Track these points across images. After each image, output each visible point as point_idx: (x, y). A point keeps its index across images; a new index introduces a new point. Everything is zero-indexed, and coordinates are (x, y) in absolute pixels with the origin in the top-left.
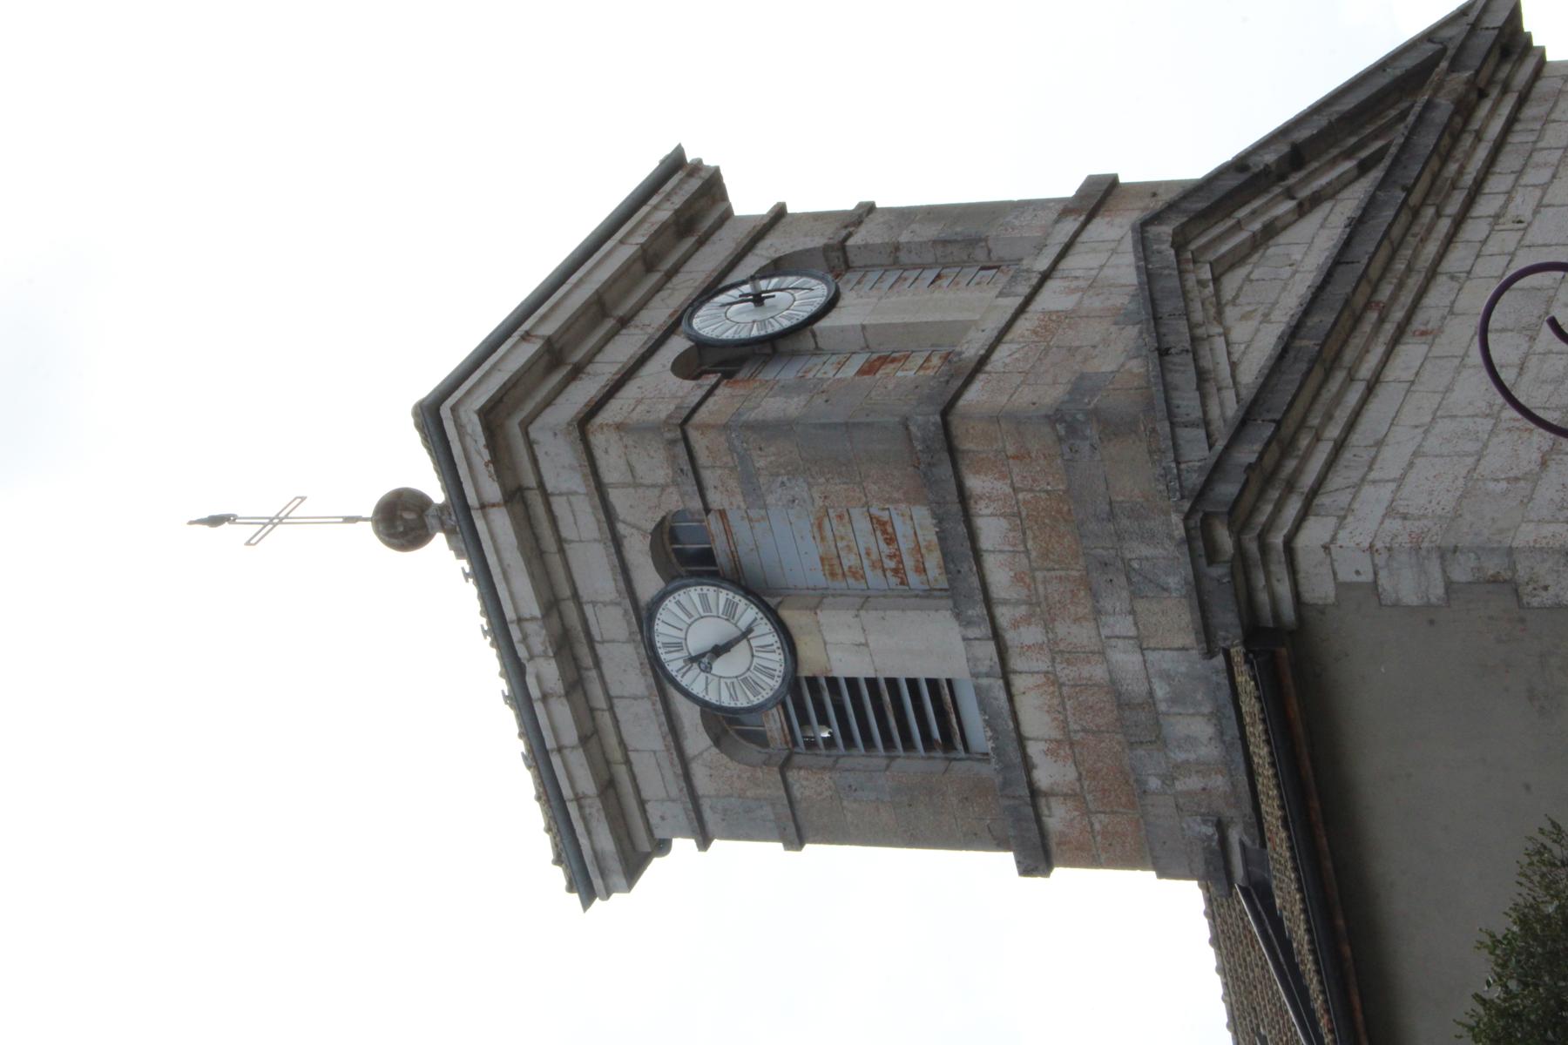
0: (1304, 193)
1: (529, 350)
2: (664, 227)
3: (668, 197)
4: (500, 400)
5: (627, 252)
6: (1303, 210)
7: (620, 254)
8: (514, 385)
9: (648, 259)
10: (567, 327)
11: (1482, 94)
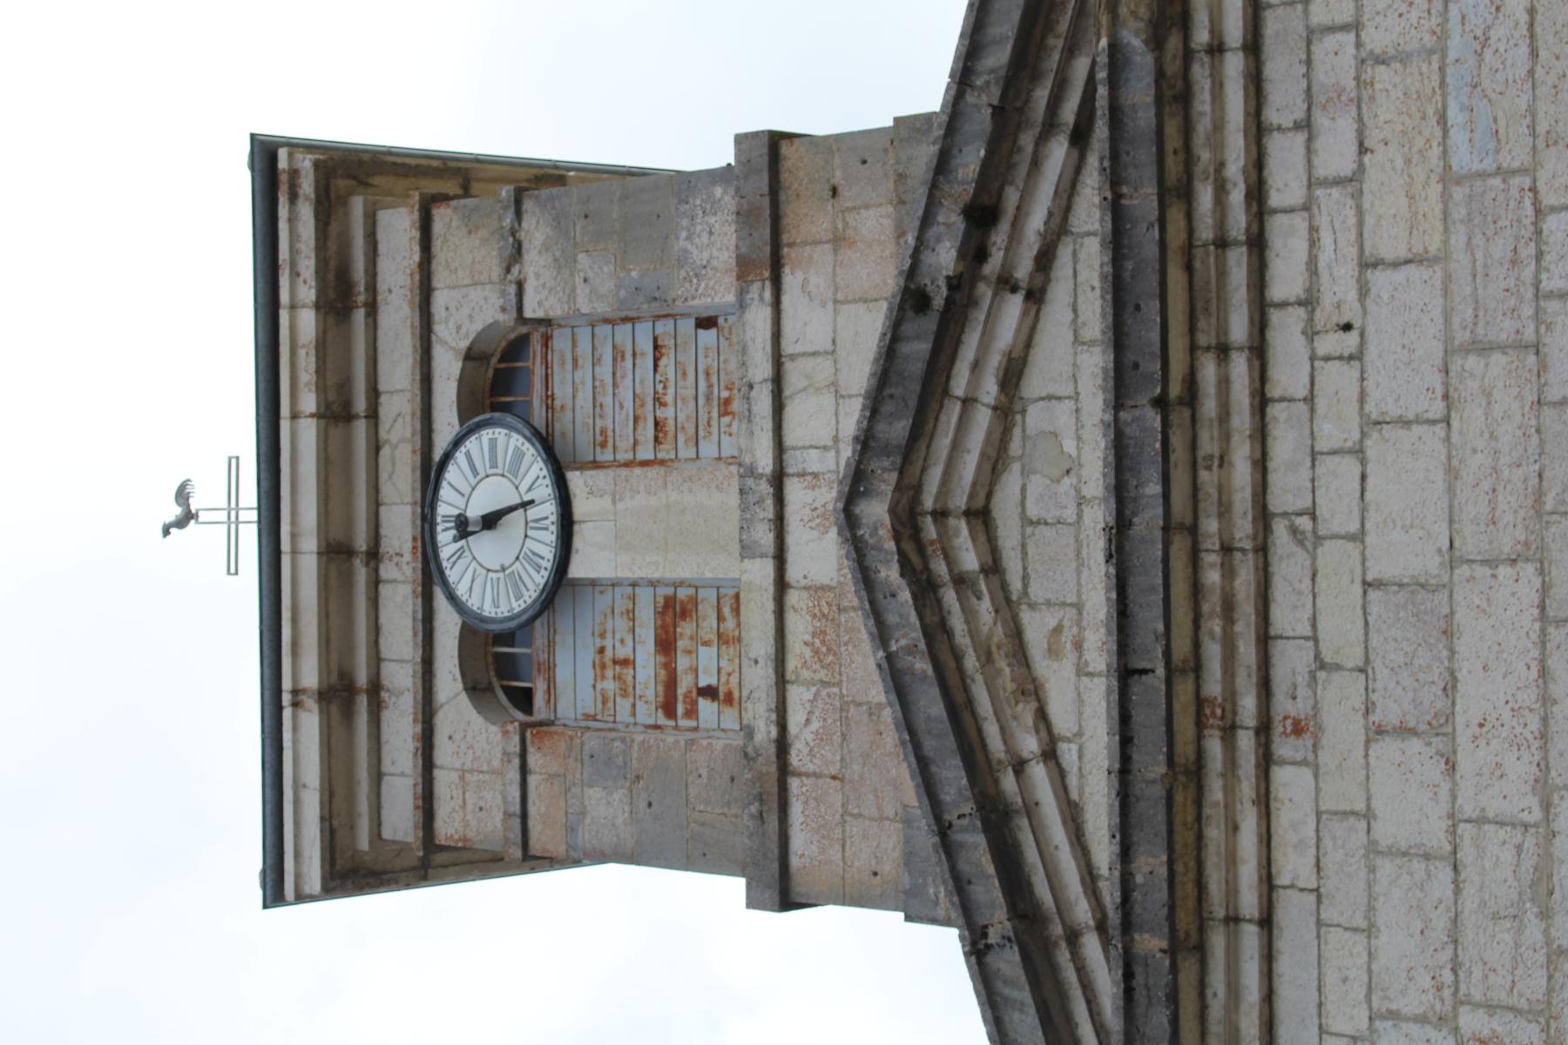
2: (321, 345)
8: (331, 794)
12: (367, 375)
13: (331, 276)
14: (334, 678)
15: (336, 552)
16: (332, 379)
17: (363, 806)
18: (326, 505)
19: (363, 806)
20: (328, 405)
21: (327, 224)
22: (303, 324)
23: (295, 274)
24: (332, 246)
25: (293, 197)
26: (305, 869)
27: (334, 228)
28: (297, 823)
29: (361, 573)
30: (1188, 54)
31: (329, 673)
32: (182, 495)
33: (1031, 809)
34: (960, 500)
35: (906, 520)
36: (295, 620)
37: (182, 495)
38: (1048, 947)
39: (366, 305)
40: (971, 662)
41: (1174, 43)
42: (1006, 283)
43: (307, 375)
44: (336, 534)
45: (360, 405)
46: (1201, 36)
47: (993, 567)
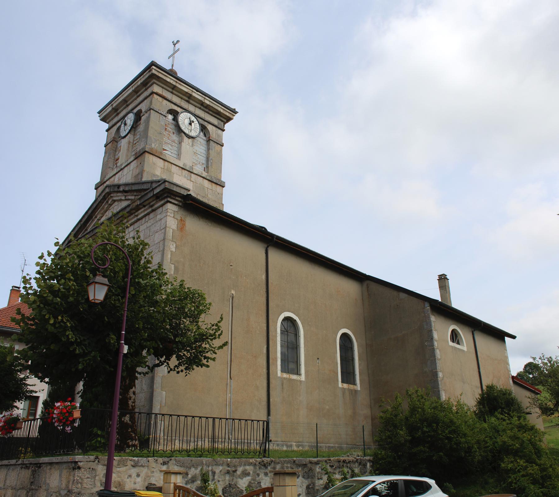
0: (127, 198)
1: (110, 109)
2: (138, 86)
5: (131, 91)
6: (126, 200)
7: (130, 90)
11: (144, 206)
25: (149, 72)
33: (93, 220)
34: (115, 199)
35: (109, 193)
41: (134, 211)
46: (136, 214)
47: (111, 205)
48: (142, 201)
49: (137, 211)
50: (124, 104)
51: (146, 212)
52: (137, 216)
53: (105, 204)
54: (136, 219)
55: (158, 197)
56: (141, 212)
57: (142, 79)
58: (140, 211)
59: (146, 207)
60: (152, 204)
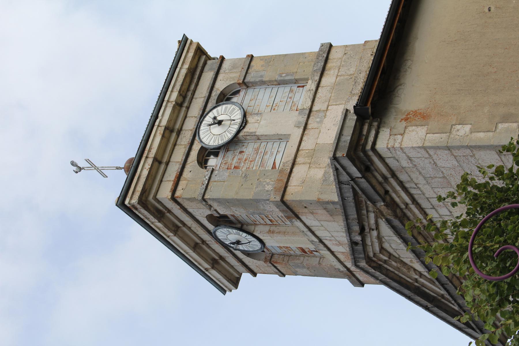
0: (374, 227)
2: (166, 226)
3: (148, 219)
4: (230, 280)
5: (176, 239)
6: (377, 228)
8: (226, 276)
9: (176, 229)
10: (206, 260)
11: (387, 192)
12: (179, 221)
13: (156, 213)
14: (211, 262)
15: (195, 247)
16: (171, 226)
17: (231, 271)
18: (183, 239)
19: (231, 271)
20: (174, 231)
21: (148, 208)
22: (158, 225)
23: (148, 219)
24: (152, 209)
25: (136, 209)
26: (229, 287)
27: (150, 207)
28: (222, 283)
29: (204, 247)
30: (401, 209)
31: (210, 263)
32: (73, 164)
33: (423, 285)
34: (377, 249)
35: (369, 260)
36: (196, 261)
37: (73, 164)
38: (439, 301)
39: (168, 212)
40: (397, 272)
41: (398, 211)
42: (371, 229)
43: (166, 231)
44: (193, 244)
45: (180, 225)
46: (403, 206)
47: (390, 255)
48: (377, 197)
49: (398, 206)
50: (201, 248)
51: (398, 188)
52: (407, 205)
53: (390, 265)
54: (413, 207)
55: (366, 169)
56: (399, 197)
57: (151, 220)
58: (397, 200)
59: (388, 188)
60: (380, 179)
